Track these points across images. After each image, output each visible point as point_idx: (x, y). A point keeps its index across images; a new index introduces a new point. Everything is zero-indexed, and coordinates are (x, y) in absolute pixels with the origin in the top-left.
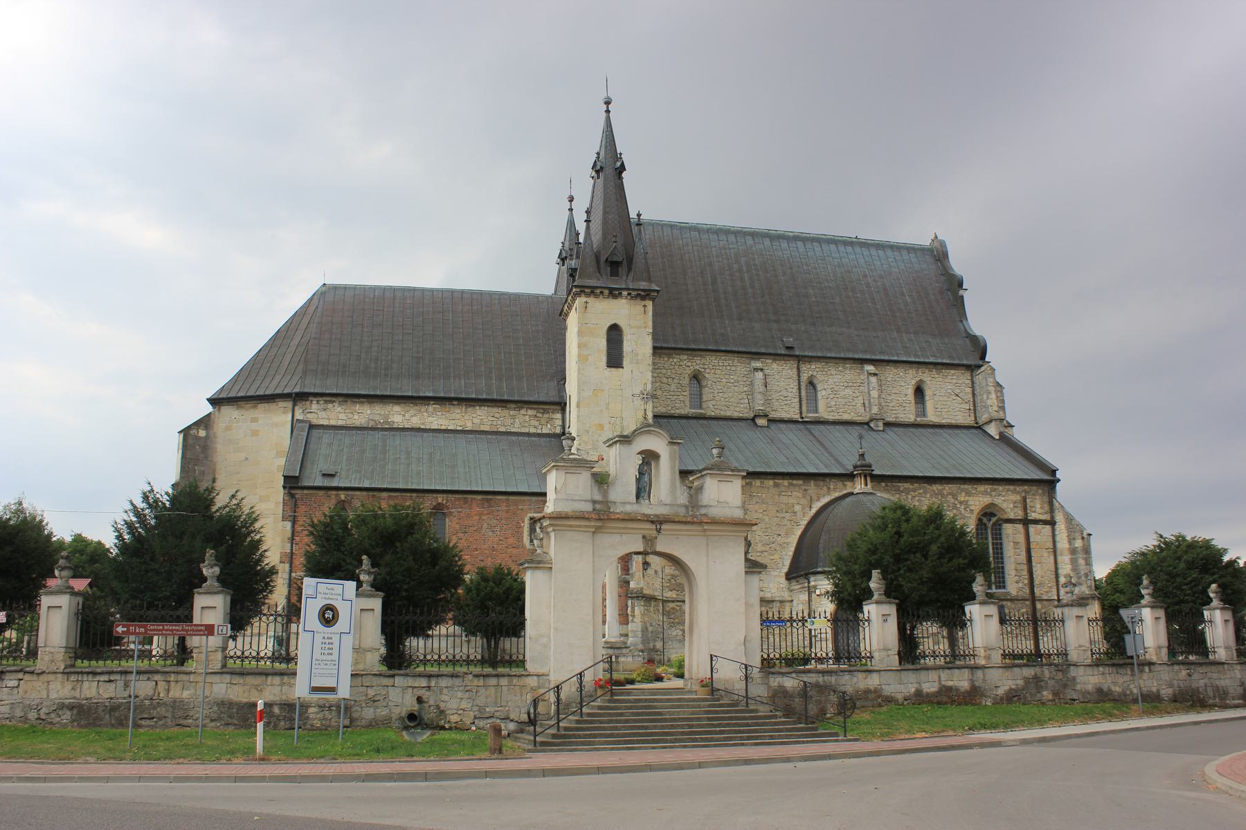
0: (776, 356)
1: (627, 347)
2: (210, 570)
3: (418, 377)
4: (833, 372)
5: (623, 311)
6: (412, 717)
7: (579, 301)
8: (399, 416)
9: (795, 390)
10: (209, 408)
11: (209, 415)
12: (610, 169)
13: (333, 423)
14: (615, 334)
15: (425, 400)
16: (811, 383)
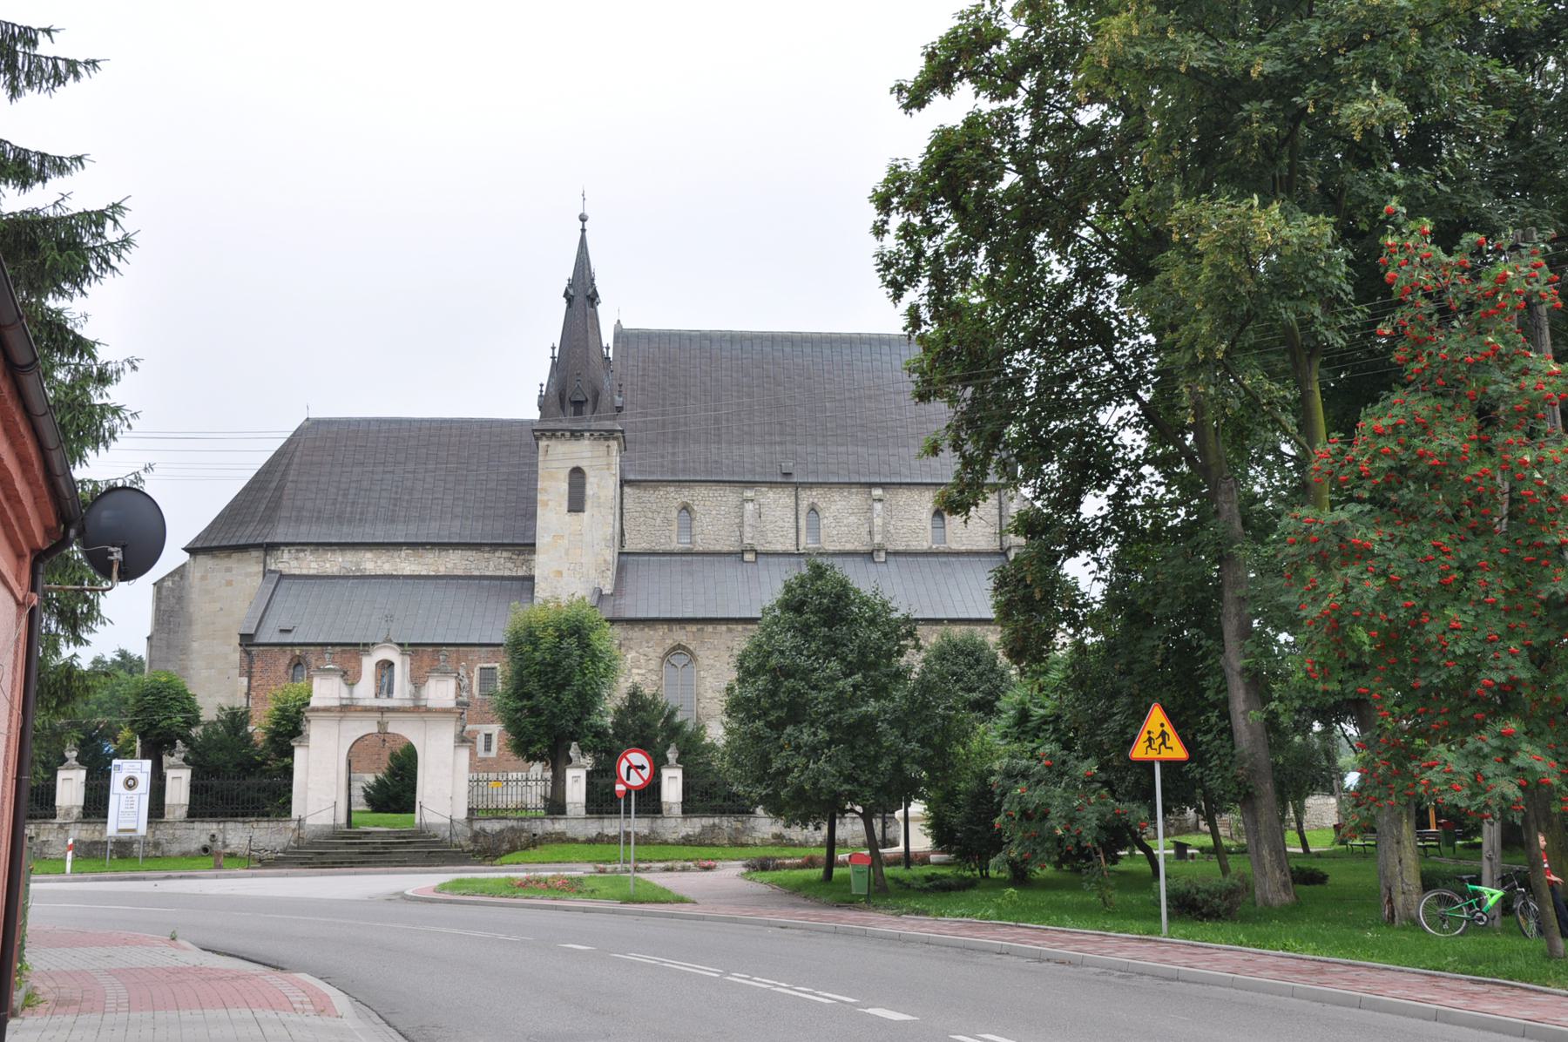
0: (772, 484)
1: (590, 490)
2: (72, 754)
3: (393, 521)
4: (837, 498)
5: (583, 452)
6: (205, 849)
7: (543, 443)
8: (371, 563)
9: (792, 519)
10: (186, 556)
11: (184, 566)
12: (582, 296)
13: (305, 572)
14: (577, 475)
15: (397, 546)
16: (813, 509)
